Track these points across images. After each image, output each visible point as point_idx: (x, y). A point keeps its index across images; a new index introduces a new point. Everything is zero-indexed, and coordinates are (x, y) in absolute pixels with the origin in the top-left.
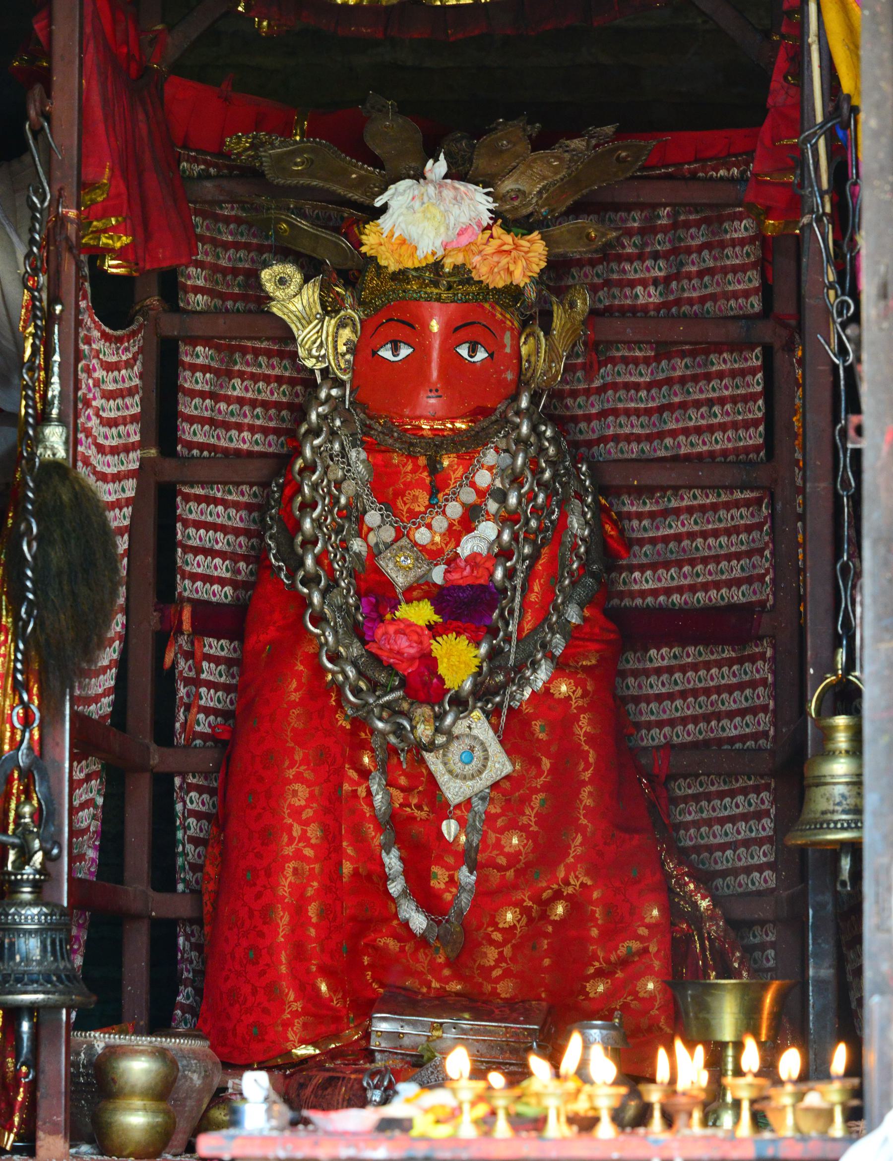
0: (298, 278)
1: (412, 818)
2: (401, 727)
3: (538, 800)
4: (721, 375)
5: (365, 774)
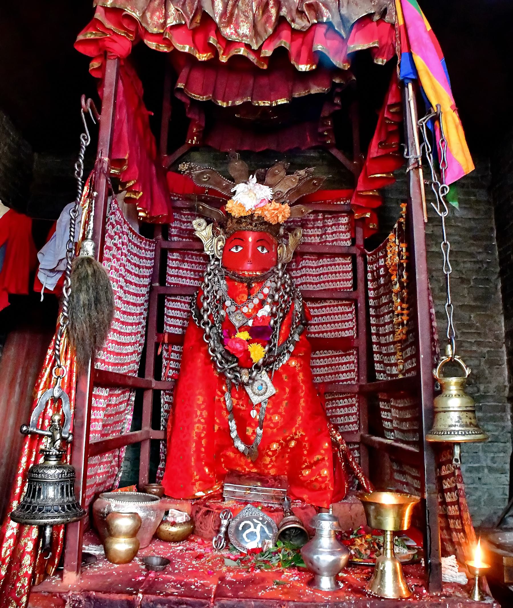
0: (205, 224)
1: (240, 409)
2: (237, 376)
3: (285, 403)
4: (339, 264)
5: (223, 393)
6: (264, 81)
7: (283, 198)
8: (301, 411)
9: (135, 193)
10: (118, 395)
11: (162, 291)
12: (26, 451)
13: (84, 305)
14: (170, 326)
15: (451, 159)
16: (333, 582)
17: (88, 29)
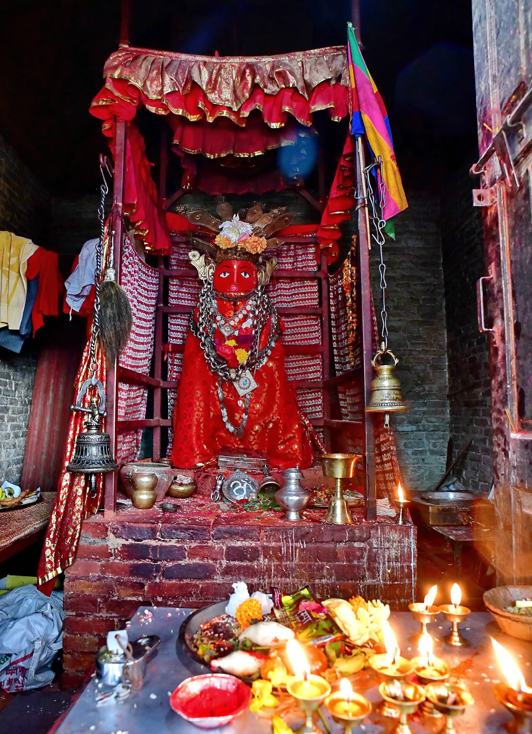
0: (198, 255)
4: (307, 286)
5: (216, 388)
6: (243, 136)
7: (260, 233)
8: (277, 401)
9: (142, 231)
10: (135, 391)
11: (166, 310)
12: (72, 426)
13: (110, 317)
14: (173, 338)
15: (389, 199)
16: (298, 516)
17: (99, 98)
